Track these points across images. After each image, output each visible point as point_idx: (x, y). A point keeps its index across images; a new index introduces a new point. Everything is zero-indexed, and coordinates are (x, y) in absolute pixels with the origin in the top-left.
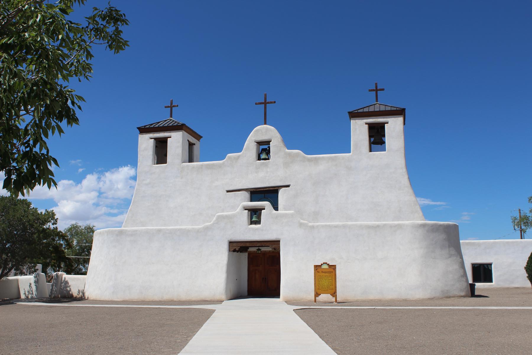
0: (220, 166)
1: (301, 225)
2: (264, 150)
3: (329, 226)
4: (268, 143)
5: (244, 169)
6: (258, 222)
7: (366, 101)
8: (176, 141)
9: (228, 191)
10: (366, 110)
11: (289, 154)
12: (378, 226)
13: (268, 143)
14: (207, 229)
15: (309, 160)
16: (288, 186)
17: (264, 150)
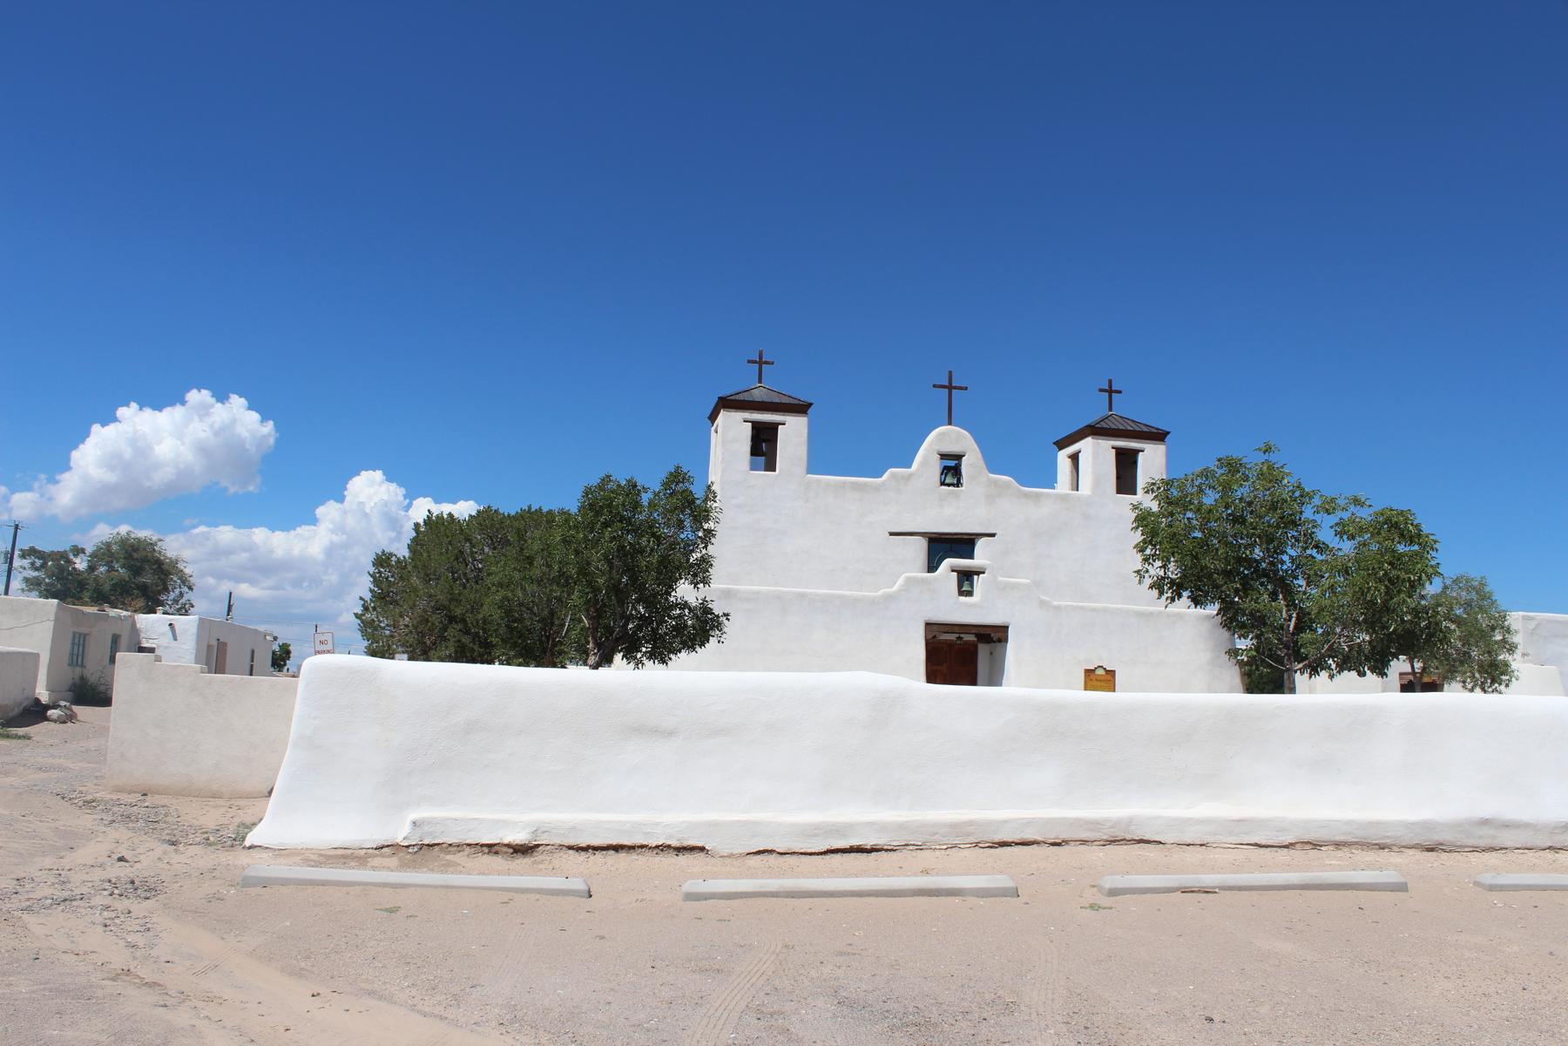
0: (877, 488)
1: (1042, 603)
2: (952, 470)
3: (1083, 608)
4: (959, 457)
5: (913, 498)
6: (970, 593)
7: (741, 381)
8: (793, 433)
9: (892, 534)
10: (740, 397)
11: (995, 482)
12: (1151, 614)
13: (959, 457)
14: (889, 598)
15: (1027, 495)
16: (993, 535)
17: (952, 470)
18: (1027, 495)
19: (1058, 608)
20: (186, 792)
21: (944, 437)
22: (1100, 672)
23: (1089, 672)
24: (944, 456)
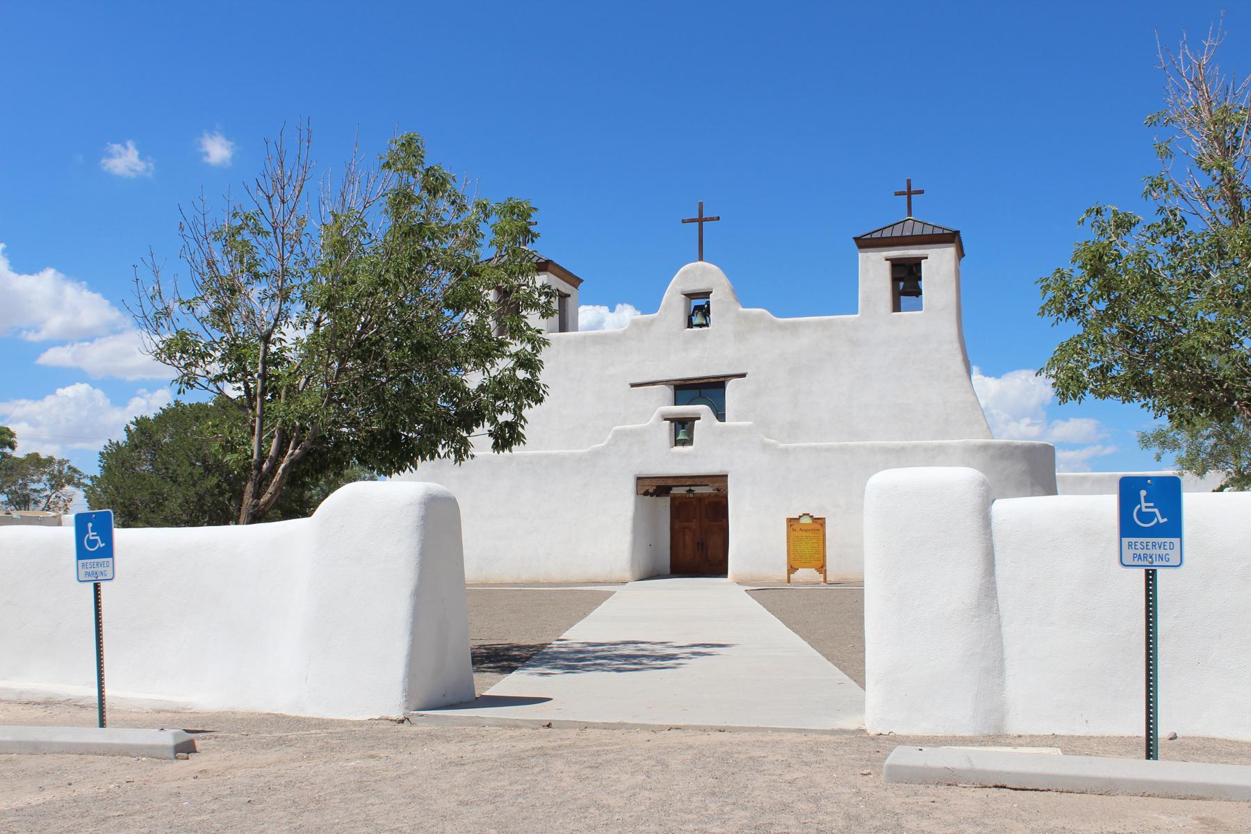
1: (765, 447)
2: (698, 309)
3: (816, 449)
4: (706, 294)
6: (688, 442)
8: (938, 264)
9: (633, 385)
11: (745, 317)
12: (903, 449)
13: (706, 294)
14: (597, 454)
15: (783, 327)
16: (743, 375)
17: (698, 309)
18: (783, 327)
19: (786, 451)
20: (508, 649)
21: (699, 274)
22: (806, 520)
23: (791, 522)
24: (690, 296)
